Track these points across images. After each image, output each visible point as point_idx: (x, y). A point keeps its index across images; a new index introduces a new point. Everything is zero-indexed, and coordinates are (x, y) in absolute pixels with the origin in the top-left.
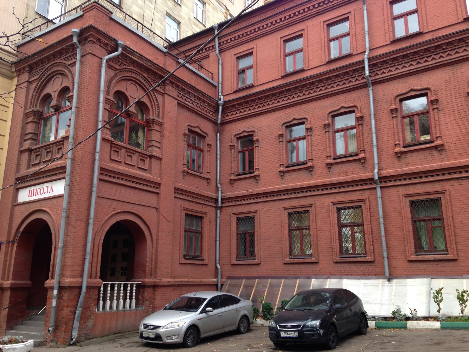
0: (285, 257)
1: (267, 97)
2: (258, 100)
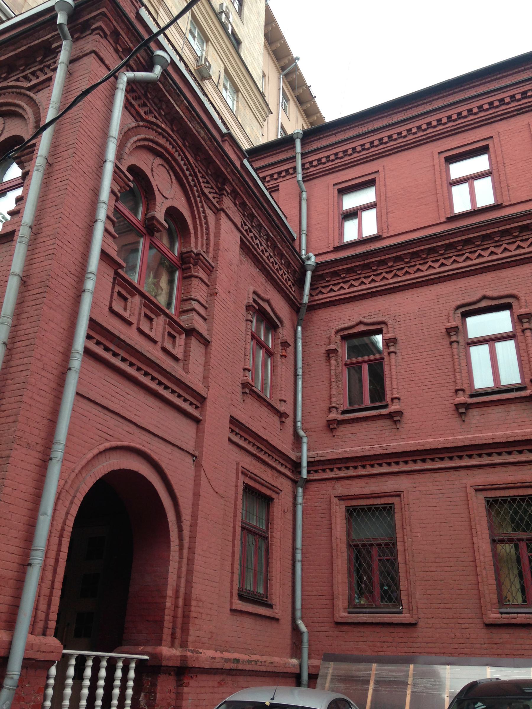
0: (489, 608)
1: (415, 255)
2: (394, 262)
